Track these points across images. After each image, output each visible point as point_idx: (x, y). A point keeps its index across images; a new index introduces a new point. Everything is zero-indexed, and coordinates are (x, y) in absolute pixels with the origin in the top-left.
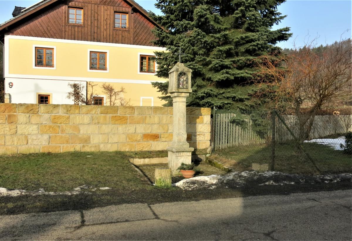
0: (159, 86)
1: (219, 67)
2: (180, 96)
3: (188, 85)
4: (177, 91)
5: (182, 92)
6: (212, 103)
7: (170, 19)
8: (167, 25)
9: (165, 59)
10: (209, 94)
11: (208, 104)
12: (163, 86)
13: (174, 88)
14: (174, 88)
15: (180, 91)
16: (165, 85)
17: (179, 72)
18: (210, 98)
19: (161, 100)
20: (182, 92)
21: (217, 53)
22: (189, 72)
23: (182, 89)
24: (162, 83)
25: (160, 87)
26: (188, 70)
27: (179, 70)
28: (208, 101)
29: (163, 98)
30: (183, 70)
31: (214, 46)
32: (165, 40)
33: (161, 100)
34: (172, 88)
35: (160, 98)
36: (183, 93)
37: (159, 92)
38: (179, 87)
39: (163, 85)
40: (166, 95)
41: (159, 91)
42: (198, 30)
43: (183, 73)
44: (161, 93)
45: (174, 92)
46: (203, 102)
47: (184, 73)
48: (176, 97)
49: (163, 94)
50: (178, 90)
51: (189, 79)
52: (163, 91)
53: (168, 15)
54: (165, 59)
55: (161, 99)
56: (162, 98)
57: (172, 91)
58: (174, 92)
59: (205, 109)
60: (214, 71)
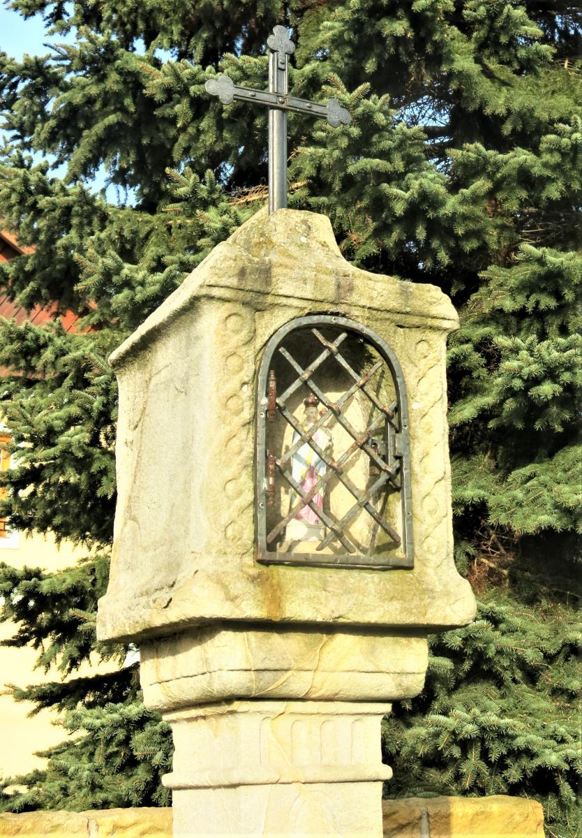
0: (17, 598)
1: (554, 409)
2: (298, 684)
3: (409, 516)
4: (251, 609)
5: (330, 628)
6: (520, 742)
7: (120, 72)
8: (89, 126)
9: (68, 382)
10: (480, 656)
11: (484, 755)
12: (46, 601)
13: (207, 563)
14: (207, 563)
15: (297, 609)
16: (62, 588)
17: (277, 323)
18: (479, 690)
19: (36, 711)
20: (330, 628)
21: (521, 299)
22: (422, 323)
23: (333, 576)
24: (37, 575)
25: (24, 603)
26: (404, 293)
27: (284, 285)
28: (483, 729)
29: (50, 697)
30: (330, 292)
31: (484, 247)
32: (73, 233)
33: (36, 711)
34: (173, 565)
35: (22, 696)
36: (341, 639)
37: (13, 649)
38: (271, 547)
39: (45, 587)
40: (75, 675)
41: (19, 641)
42: (367, 96)
43: (331, 331)
44: (29, 653)
45: (200, 629)
46: (437, 735)
47: (353, 334)
48: (229, 699)
49: (46, 663)
50: (275, 595)
51: (417, 426)
52: (47, 642)
53: (101, 38)
54: (68, 382)
55: (36, 704)
56: (39, 698)
57: (174, 615)
58: (200, 629)
59: (486, 815)
60: (494, 457)
